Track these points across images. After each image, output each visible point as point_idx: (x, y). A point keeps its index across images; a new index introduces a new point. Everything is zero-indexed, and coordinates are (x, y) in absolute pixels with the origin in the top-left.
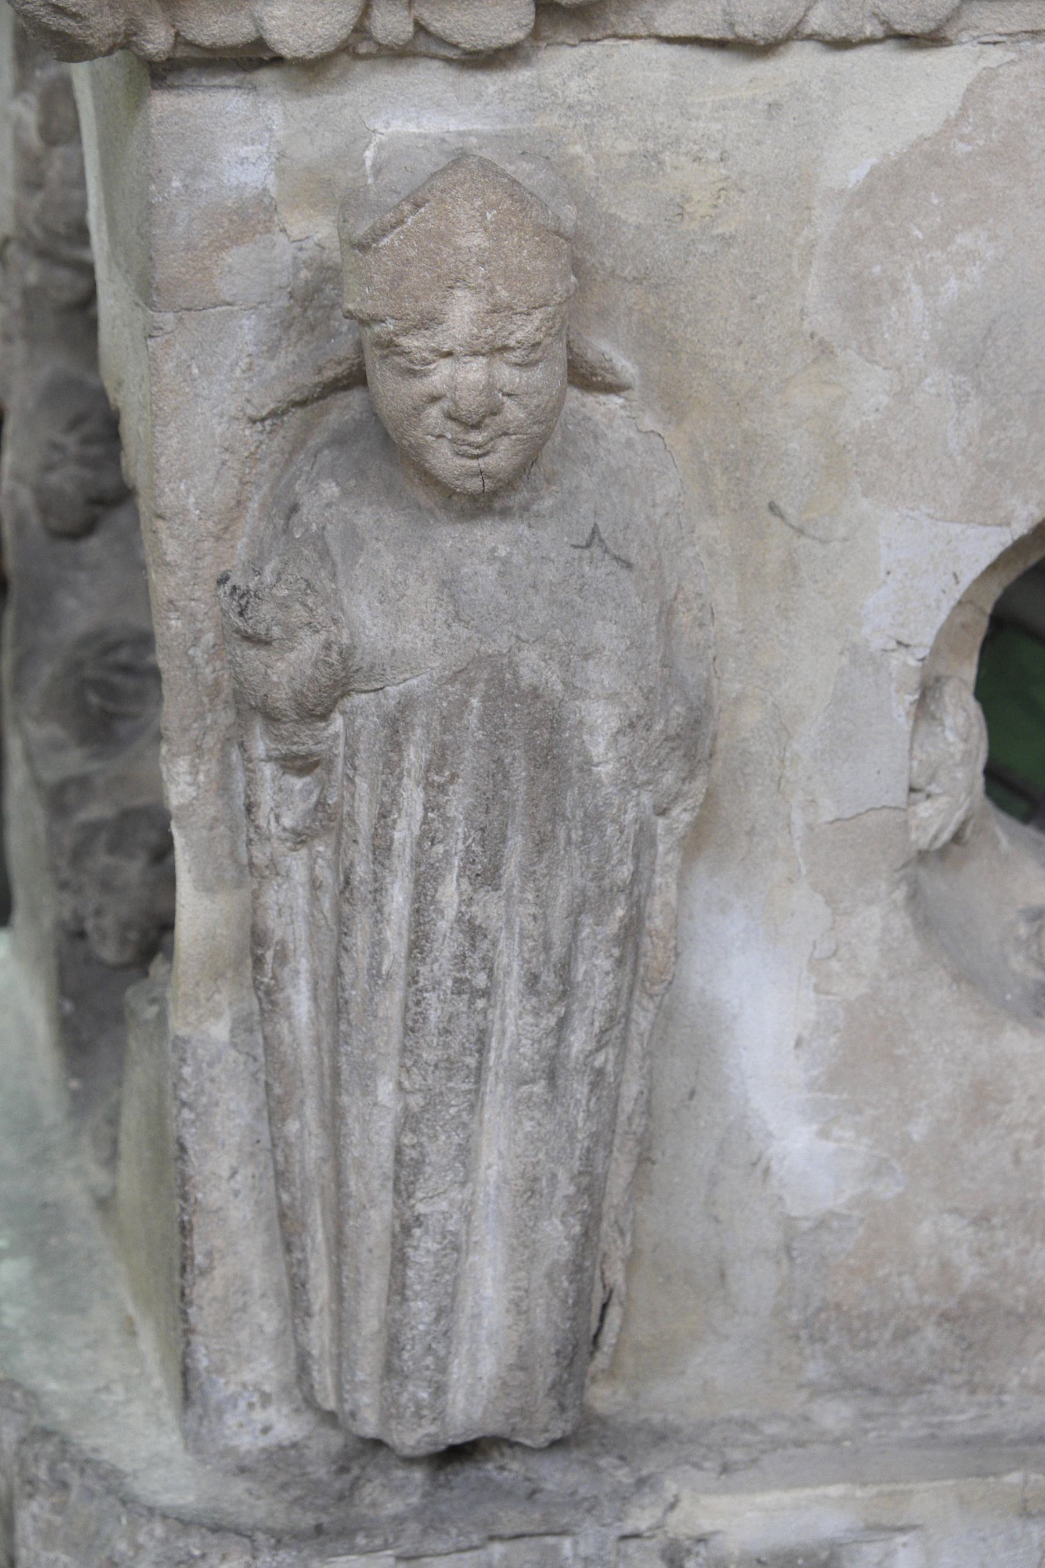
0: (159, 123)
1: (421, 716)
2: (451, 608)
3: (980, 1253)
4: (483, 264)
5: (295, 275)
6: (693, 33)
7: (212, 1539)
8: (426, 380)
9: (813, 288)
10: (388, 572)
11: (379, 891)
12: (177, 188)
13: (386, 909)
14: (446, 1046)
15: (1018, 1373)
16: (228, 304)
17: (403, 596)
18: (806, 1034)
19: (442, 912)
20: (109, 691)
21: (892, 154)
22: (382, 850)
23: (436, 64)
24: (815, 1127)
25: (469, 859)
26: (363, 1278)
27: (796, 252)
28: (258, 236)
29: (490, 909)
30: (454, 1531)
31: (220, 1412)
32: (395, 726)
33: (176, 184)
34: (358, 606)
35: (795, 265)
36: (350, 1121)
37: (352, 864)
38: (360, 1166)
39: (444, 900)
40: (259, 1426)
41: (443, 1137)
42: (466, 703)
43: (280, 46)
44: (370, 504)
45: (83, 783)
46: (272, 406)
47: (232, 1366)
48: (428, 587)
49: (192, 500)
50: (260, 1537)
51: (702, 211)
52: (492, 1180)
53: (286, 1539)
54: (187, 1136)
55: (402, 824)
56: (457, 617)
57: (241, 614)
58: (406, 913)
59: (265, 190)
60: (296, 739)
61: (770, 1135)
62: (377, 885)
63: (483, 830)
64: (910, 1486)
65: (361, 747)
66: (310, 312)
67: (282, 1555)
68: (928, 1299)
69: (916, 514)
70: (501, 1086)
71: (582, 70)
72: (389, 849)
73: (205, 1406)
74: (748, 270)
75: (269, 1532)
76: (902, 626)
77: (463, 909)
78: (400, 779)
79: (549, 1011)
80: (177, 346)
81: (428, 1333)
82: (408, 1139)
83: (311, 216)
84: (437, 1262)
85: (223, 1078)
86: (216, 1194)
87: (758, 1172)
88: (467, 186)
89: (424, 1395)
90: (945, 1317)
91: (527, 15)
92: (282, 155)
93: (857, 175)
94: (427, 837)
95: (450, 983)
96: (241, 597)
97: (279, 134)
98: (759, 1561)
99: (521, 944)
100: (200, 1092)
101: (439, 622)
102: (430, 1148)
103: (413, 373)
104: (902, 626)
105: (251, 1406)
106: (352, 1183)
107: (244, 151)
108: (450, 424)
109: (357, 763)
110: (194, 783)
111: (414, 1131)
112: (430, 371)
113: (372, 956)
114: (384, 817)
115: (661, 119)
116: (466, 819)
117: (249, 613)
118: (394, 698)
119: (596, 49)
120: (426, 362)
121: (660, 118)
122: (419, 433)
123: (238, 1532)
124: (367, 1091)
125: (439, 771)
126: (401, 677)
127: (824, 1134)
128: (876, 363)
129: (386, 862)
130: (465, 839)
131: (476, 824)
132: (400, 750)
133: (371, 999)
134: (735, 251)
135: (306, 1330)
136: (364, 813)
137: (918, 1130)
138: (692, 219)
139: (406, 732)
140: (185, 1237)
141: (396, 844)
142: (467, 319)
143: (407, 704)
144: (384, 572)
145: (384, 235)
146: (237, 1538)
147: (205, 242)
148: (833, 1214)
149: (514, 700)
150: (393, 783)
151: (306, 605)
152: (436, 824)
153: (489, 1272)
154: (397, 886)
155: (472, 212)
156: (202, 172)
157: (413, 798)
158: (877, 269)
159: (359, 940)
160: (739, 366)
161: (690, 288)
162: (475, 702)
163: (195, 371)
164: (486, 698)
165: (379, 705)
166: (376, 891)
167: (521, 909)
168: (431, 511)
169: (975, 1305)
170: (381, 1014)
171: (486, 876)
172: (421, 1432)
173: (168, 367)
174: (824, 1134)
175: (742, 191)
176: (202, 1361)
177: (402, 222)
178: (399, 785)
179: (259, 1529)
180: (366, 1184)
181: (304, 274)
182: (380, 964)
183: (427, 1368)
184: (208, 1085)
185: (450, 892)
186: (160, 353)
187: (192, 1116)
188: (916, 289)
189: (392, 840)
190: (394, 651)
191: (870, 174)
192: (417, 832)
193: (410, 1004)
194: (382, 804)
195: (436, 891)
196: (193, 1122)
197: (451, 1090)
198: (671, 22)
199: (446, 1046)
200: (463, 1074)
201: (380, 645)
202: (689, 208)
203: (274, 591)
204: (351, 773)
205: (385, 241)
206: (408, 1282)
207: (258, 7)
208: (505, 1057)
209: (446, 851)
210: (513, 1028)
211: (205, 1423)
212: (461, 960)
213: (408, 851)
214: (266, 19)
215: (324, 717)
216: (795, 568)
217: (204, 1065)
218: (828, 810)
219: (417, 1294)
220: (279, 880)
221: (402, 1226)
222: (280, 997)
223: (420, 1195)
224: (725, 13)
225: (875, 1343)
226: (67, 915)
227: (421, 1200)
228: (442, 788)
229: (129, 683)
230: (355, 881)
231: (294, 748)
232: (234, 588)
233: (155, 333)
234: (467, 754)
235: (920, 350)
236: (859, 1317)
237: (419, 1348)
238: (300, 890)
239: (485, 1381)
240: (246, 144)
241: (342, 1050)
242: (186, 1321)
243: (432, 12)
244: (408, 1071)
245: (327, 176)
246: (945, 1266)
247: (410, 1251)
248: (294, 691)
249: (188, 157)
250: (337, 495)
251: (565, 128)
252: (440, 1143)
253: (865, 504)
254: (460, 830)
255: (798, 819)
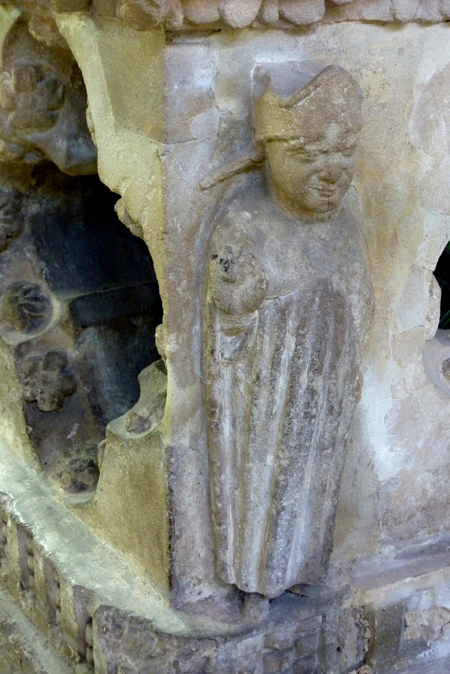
0: (169, 60)
1: (294, 308)
2: (308, 261)
3: (434, 484)
4: (344, 112)
5: (220, 126)
6: (378, 19)
7: (199, 643)
8: (313, 164)
9: (411, 124)
10: (279, 249)
11: (273, 380)
12: (176, 89)
13: (276, 388)
14: (300, 439)
15: (443, 524)
16: (195, 140)
17: (287, 258)
18: (388, 414)
19: (301, 386)
20: (32, 309)
21: (440, 69)
22: (275, 363)
23: (280, 32)
24: (389, 448)
25: (313, 363)
26: (255, 533)
27: (406, 110)
28: (207, 109)
29: (319, 384)
30: (286, 622)
31: (183, 589)
32: (283, 313)
33: (176, 87)
34: (267, 263)
35: (405, 115)
36: (253, 473)
37: (261, 371)
38: (256, 490)
39: (302, 381)
40: (197, 592)
41: (295, 475)
42: (313, 300)
43: (231, 22)
44: (267, 220)
45: (28, 343)
46: (212, 182)
47: (188, 571)
48: (297, 254)
49: (179, 225)
50: (218, 639)
51: (375, 93)
52: (308, 488)
53: (228, 638)
54: (173, 485)
55: (285, 352)
56: (311, 265)
57: (226, 271)
58: (285, 388)
59: (210, 89)
60: (238, 321)
61: (375, 453)
62: (272, 378)
63: (319, 351)
64: (430, 573)
65: (267, 322)
66: (224, 142)
67: (228, 644)
68: (419, 503)
69: (436, 213)
70: (315, 452)
71: (334, 34)
72: (279, 363)
73: (178, 588)
74: (390, 117)
75: (221, 636)
76: (429, 256)
77: (309, 384)
78: (285, 334)
79: (336, 420)
80: (175, 159)
81: (283, 551)
82: (281, 478)
83: (228, 100)
84: (289, 524)
85: (187, 461)
86: (183, 507)
87: (370, 467)
88: (337, 77)
89: (280, 574)
90: (423, 509)
91: (322, 9)
92: (218, 74)
93: (428, 78)
94: (297, 355)
95: (302, 414)
96: (226, 263)
97: (218, 64)
98: (383, 610)
99: (328, 395)
100: (178, 467)
101: (303, 267)
102: (290, 480)
103: (308, 161)
104: (429, 256)
105: (195, 585)
106: (252, 497)
107: (203, 72)
108: (321, 182)
109: (265, 329)
110: (178, 343)
111: (285, 475)
112: (316, 160)
113: (268, 407)
114: (278, 350)
115: (362, 55)
116: (312, 347)
117: (229, 271)
118: (284, 301)
119: (339, 26)
120: (316, 155)
121: (362, 55)
122: (306, 187)
123: (209, 639)
124: (262, 460)
125: (303, 329)
126: (287, 292)
127: (391, 450)
128: (429, 154)
129: (278, 368)
130: (312, 356)
131: (316, 349)
132: (286, 322)
133: (267, 424)
134: (386, 110)
135: (225, 555)
136: (268, 350)
137: (420, 444)
138: (371, 97)
139: (288, 315)
140: (171, 525)
141: (282, 361)
142: (335, 136)
143: (288, 304)
144: (276, 249)
145: (300, 101)
146: (209, 641)
147: (187, 113)
148: (393, 478)
149: (331, 298)
150: (282, 336)
151: (252, 265)
152: (301, 351)
153: (304, 523)
154: (281, 378)
155: (339, 89)
156: (186, 81)
157: (291, 341)
158: (432, 116)
159: (262, 401)
160: (384, 157)
161: (369, 125)
162: (317, 299)
163: (181, 169)
164: (321, 297)
165: (276, 304)
166: (272, 380)
167: (329, 381)
168: (294, 221)
169: (432, 502)
170: (270, 430)
171: (316, 369)
172: (278, 588)
173: (171, 168)
174: (391, 450)
175: (390, 85)
176: (178, 571)
177: (309, 94)
178: (284, 337)
179: (217, 636)
180: (259, 496)
181: (223, 125)
182: (272, 410)
183: (282, 564)
184: (181, 464)
185: (304, 379)
186: (167, 162)
187: (175, 477)
188: (444, 123)
189: (281, 359)
190: (284, 281)
191: (433, 77)
192: (291, 354)
193: (286, 424)
194: (277, 345)
195: (299, 378)
196: (176, 479)
197: (299, 456)
198: (370, 13)
199: (300, 439)
200: (305, 449)
201: (278, 279)
202: (371, 92)
203: (239, 260)
204: (261, 333)
205: (300, 104)
206: (277, 533)
207: (222, 5)
208: (317, 440)
209: (304, 362)
210: (322, 429)
211: (178, 595)
212: (308, 405)
213: (287, 363)
214: (226, 10)
215: (252, 311)
216: (396, 237)
217: (180, 457)
218: (401, 329)
219: (280, 537)
220: (220, 379)
221: (277, 512)
222: (220, 426)
223: (285, 499)
224: (391, 9)
225: (402, 522)
226: (28, 394)
227: (285, 501)
228: (303, 336)
229: (38, 305)
230: (262, 377)
231: (237, 325)
232: (221, 260)
233: (166, 153)
234: (313, 321)
235: (443, 148)
236: (398, 514)
237: (279, 557)
238: (227, 382)
239: (298, 564)
240: (204, 69)
241: (251, 445)
242: (172, 557)
243: (287, 8)
244: (283, 451)
245: (235, 82)
246: (424, 490)
247: (279, 521)
248: (243, 302)
249: (181, 75)
250: (250, 217)
251: (326, 60)
252: (294, 477)
253: (421, 209)
254: (309, 352)
255: (390, 333)
